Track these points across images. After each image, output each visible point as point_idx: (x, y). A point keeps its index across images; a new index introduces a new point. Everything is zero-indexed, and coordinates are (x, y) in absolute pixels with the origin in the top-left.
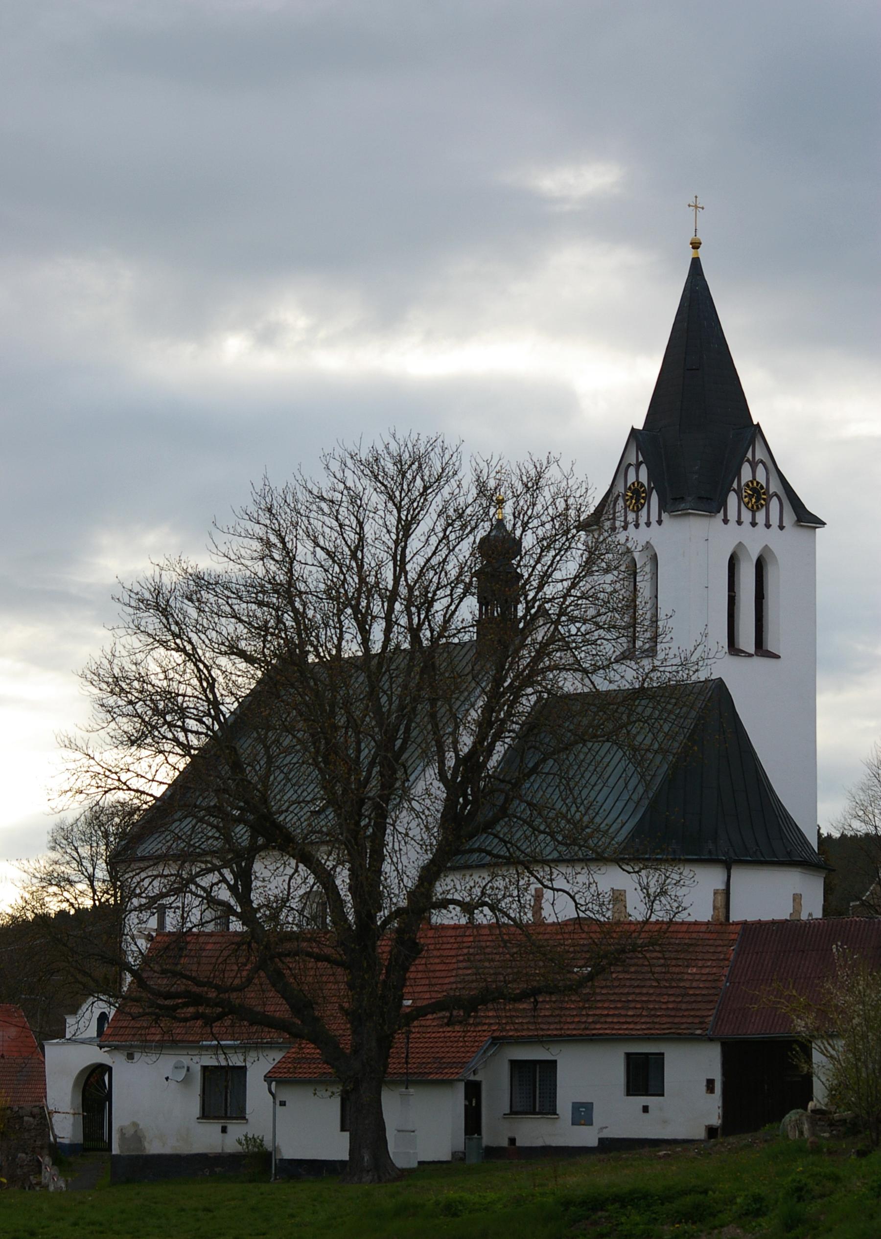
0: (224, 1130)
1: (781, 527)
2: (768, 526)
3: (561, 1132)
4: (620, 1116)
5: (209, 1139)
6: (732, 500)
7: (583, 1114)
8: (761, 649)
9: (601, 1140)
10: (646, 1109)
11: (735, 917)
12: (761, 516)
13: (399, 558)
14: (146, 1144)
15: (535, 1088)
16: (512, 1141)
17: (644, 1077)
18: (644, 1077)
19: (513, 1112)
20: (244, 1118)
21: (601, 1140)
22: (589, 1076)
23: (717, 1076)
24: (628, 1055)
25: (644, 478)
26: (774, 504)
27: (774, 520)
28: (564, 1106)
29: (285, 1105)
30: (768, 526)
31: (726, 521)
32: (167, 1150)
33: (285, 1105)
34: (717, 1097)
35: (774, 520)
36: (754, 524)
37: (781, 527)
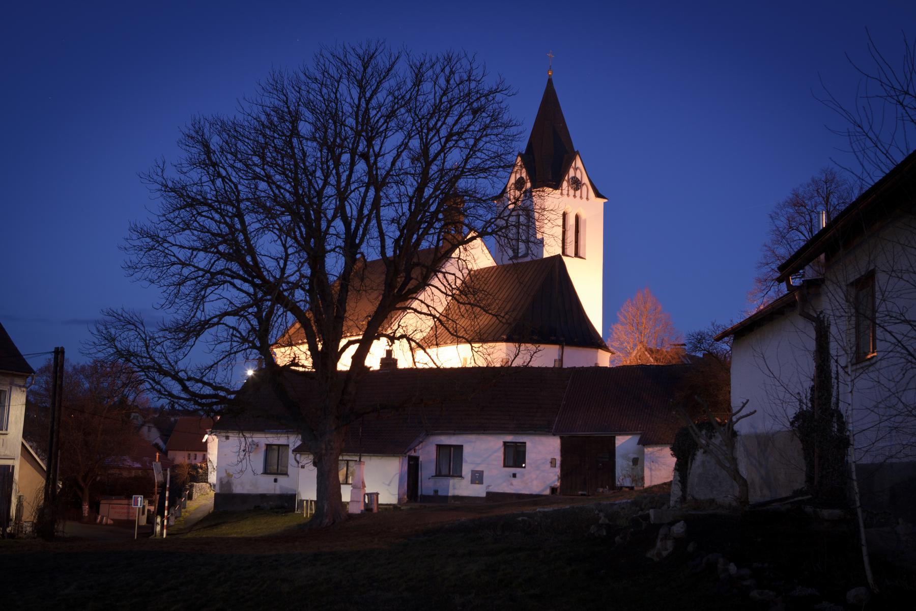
0: (276, 481)
1: (587, 199)
2: (581, 197)
3: (462, 488)
4: (500, 480)
5: (266, 485)
6: (565, 184)
7: (478, 477)
8: (577, 255)
9: (488, 493)
10: (514, 475)
11: (565, 366)
12: (578, 193)
13: (360, 120)
14: (234, 488)
15: (451, 459)
16: (436, 491)
17: (515, 457)
18: (515, 457)
19: (436, 476)
20: (461, 476)
21: (488, 493)
22: (483, 453)
23: (558, 458)
24: (505, 443)
25: (524, 175)
26: (584, 188)
27: (584, 195)
28: (466, 470)
29: (481, 473)
30: (581, 197)
31: (562, 194)
32: (245, 492)
33: (481, 473)
34: (558, 470)
35: (584, 195)
36: (575, 196)
37: (587, 199)
